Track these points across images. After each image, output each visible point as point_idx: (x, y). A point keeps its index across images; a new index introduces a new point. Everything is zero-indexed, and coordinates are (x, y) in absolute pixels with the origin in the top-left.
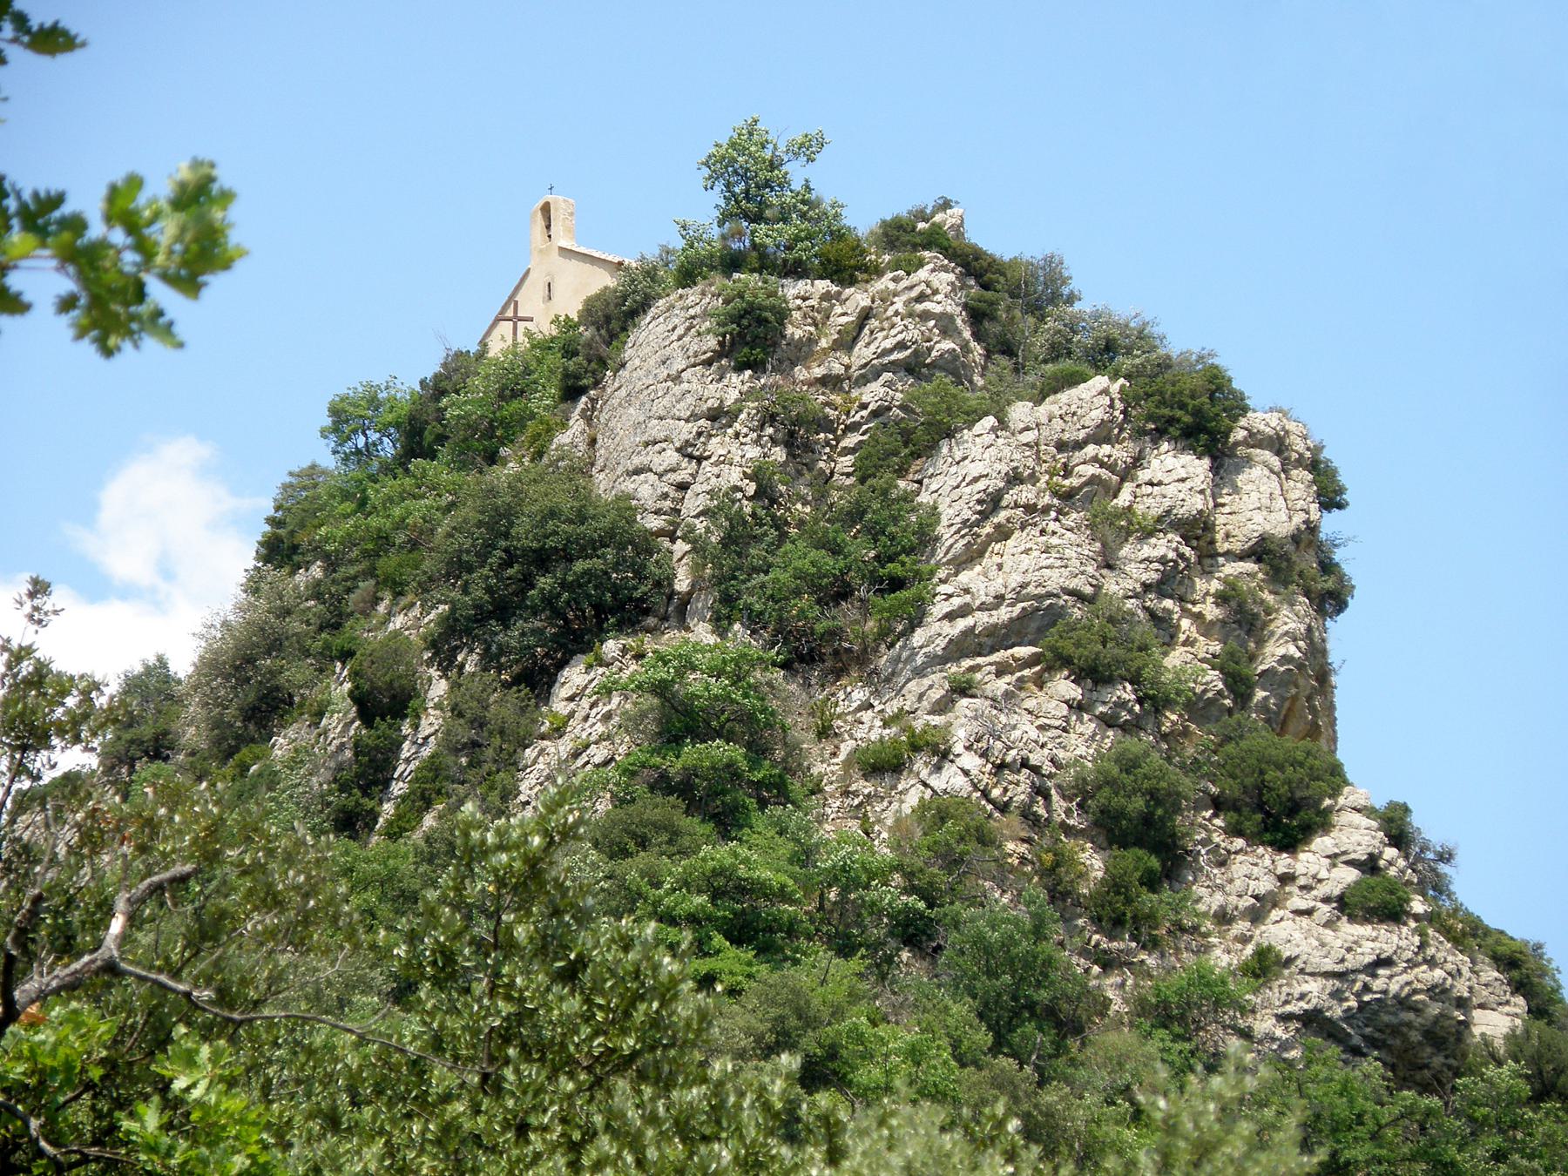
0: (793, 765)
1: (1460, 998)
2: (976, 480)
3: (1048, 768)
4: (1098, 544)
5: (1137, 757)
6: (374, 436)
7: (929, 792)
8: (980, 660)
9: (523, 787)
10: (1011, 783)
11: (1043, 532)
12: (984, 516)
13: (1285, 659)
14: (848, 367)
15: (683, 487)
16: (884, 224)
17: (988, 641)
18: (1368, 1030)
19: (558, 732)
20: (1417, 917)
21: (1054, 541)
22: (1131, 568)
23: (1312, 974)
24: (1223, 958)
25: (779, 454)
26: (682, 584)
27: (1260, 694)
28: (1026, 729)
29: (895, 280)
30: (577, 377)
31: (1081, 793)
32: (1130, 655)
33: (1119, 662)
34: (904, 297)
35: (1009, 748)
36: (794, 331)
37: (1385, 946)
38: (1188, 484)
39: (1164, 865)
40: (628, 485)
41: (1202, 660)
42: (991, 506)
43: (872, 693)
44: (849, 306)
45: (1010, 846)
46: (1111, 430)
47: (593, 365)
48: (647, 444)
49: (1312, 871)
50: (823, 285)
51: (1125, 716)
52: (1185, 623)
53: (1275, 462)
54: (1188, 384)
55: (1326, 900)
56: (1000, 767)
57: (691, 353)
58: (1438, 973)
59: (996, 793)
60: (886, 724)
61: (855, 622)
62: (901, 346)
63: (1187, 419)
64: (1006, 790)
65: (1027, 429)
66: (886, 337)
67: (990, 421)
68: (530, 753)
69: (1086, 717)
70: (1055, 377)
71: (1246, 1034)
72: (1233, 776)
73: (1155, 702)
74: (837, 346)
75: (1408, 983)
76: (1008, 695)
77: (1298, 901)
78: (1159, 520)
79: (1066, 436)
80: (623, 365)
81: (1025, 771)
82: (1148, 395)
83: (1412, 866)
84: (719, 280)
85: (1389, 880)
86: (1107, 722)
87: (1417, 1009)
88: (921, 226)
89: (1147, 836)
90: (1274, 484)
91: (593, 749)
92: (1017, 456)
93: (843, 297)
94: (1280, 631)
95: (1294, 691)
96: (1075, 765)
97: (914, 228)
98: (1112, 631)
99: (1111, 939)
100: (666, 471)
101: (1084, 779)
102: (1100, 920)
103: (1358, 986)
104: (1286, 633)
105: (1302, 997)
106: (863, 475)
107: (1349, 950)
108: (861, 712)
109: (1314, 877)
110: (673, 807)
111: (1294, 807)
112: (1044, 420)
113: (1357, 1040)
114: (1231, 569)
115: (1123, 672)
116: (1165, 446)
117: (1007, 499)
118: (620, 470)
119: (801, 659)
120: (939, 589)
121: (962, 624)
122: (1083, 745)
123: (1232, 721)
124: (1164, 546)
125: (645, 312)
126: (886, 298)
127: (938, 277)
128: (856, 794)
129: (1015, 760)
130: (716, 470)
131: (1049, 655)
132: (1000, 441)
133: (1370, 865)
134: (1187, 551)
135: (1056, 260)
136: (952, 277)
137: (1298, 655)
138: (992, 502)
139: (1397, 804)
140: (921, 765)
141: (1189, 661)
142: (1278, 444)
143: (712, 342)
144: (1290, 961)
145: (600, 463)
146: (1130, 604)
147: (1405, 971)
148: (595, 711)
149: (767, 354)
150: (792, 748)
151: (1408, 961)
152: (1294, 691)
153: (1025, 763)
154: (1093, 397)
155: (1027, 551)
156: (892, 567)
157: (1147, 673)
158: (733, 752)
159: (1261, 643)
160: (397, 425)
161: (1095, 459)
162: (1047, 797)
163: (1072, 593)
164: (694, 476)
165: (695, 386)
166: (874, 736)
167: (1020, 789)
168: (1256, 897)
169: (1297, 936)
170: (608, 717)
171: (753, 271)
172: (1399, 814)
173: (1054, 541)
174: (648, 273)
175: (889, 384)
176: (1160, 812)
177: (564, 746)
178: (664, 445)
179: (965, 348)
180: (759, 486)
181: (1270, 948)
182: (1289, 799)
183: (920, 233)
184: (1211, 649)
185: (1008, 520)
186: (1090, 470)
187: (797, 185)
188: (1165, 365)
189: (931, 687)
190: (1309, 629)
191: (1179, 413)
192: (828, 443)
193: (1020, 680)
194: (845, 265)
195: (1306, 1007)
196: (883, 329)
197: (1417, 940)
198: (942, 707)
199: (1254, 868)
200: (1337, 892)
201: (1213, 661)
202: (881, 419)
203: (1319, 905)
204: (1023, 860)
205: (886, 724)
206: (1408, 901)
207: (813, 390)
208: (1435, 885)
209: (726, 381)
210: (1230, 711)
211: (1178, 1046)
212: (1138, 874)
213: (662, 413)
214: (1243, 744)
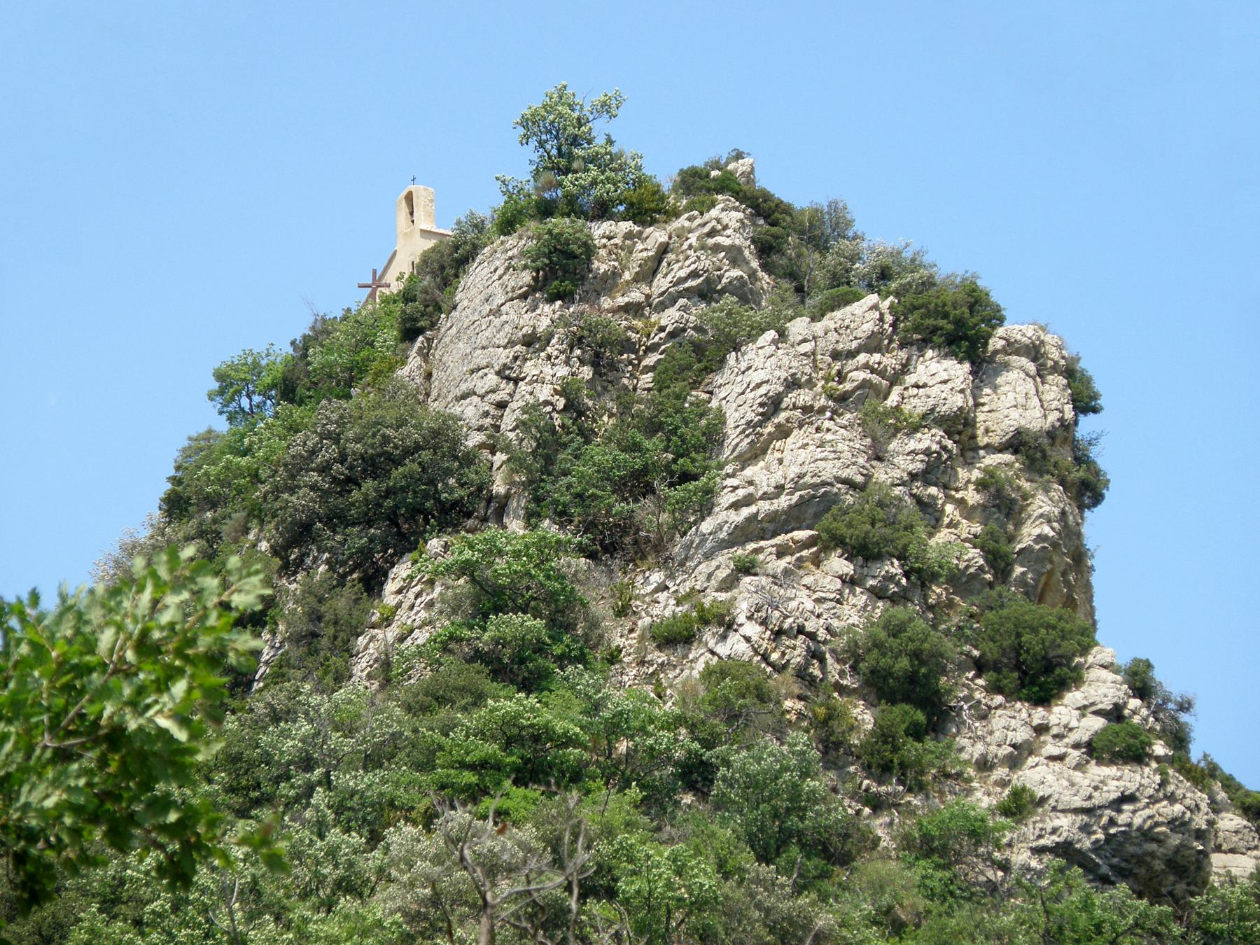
0: (593, 639)
1: (1199, 830)
2: (758, 386)
3: (822, 634)
4: (869, 440)
5: (903, 623)
6: (257, 399)
7: (716, 658)
8: (762, 543)
9: (356, 670)
10: (788, 647)
11: (818, 430)
12: (766, 417)
13: (1040, 538)
14: (648, 297)
15: (502, 405)
16: (682, 173)
17: (770, 527)
18: (1115, 860)
19: (387, 621)
20: (1158, 759)
21: (829, 437)
22: (899, 460)
23: (1063, 811)
24: (983, 799)
25: (587, 372)
26: (499, 488)
27: (1018, 570)
28: (801, 601)
29: (690, 219)
30: (416, 320)
31: (852, 657)
32: (896, 535)
33: (887, 540)
34: (697, 234)
35: (786, 617)
36: (601, 266)
37: (1128, 784)
38: (950, 385)
39: (929, 720)
40: (456, 410)
41: (964, 540)
42: (772, 408)
43: (667, 577)
44: (650, 244)
45: (788, 704)
46: (881, 341)
47: (430, 309)
48: (472, 372)
49: (1064, 721)
50: (626, 226)
51: (893, 588)
52: (949, 508)
53: (1032, 367)
54: (948, 297)
55: (1076, 746)
56: (779, 634)
57: (509, 289)
58: (1178, 808)
59: (774, 656)
60: (678, 603)
61: (649, 515)
62: (694, 274)
63: (950, 327)
64: (783, 654)
65: (805, 341)
66: (681, 268)
67: (771, 334)
68: (362, 641)
69: (858, 590)
70: (833, 298)
71: (1005, 867)
72: (992, 639)
73: (921, 577)
74: (637, 279)
75: (1150, 817)
76: (786, 572)
77: (1052, 749)
78: (924, 417)
79: (840, 347)
80: (455, 308)
81: (802, 637)
82: (915, 308)
83: (1154, 713)
84: (533, 225)
85: (1132, 726)
86: (878, 594)
87: (1158, 840)
88: (714, 173)
89: (915, 693)
90: (1030, 385)
91: (417, 633)
92: (793, 364)
93: (644, 235)
94: (1036, 514)
95: (1049, 567)
96: (848, 633)
97: (708, 175)
98: (881, 514)
99: (880, 783)
100: (487, 392)
101: (856, 643)
102: (869, 767)
103: (1104, 820)
104: (1041, 516)
105: (1054, 831)
106: (660, 385)
107: (1096, 788)
108: (658, 596)
109: (1066, 726)
110: (478, 672)
111: (1049, 666)
112: (821, 333)
113: (1105, 869)
114: (991, 460)
115: (891, 549)
116: (930, 353)
117: (787, 401)
118: (451, 396)
119: (606, 549)
120: (725, 483)
121: (746, 512)
122: (854, 615)
123: (994, 593)
124: (928, 439)
125: (473, 260)
126: (682, 234)
127: (728, 216)
128: (651, 663)
129: (791, 628)
130: (529, 388)
131: (825, 536)
132: (780, 352)
133: (1116, 714)
134: (949, 444)
135: (841, 205)
136: (740, 215)
137: (1052, 534)
138: (773, 405)
139: (1141, 661)
140: (709, 636)
141: (954, 541)
142: (1034, 351)
143: (527, 277)
144: (1043, 800)
145: (434, 394)
146: (898, 491)
147: (1147, 806)
148: (419, 600)
149: (576, 286)
150: (594, 624)
151: (1150, 797)
152: (1049, 567)
153: (801, 630)
154: (865, 314)
155: (804, 446)
156: (680, 457)
157: (912, 549)
158: (534, 624)
159: (1019, 524)
160: (273, 386)
161: (866, 366)
162: (822, 661)
163: (845, 481)
164: (511, 395)
165: (513, 316)
166: (668, 613)
167: (796, 653)
168: (1014, 746)
169: (1050, 778)
170: (430, 605)
171: (563, 215)
172: (1142, 667)
173: (829, 437)
174: (476, 226)
175: (684, 309)
176: (923, 670)
177: (391, 633)
178: (486, 371)
179: (753, 275)
180: (568, 400)
181: (1024, 789)
182: (1044, 658)
183: (714, 179)
184: (973, 530)
185: (787, 420)
186: (861, 375)
187: (600, 140)
188: (929, 283)
189: (718, 567)
190: (1063, 513)
191: (942, 322)
192: (630, 363)
193: (800, 559)
194: (645, 208)
195: (1057, 840)
196: (678, 261)
197: (1158, 778)
198: (729, 584)
199: (1011, 721)
200: (1085, 738)
201: (974, 540)
202: (677, 339)
203: (1070, 750)
204: (800, 716)
205: (678, 603)
206: (1150, 745)
207: (617, 316)
208: (1179, 739)
209: (538, 311)
210: (991, 585)
211: (939, 874)
212: (904, 726)
213: (485, 343)
214: (1005, 612)
